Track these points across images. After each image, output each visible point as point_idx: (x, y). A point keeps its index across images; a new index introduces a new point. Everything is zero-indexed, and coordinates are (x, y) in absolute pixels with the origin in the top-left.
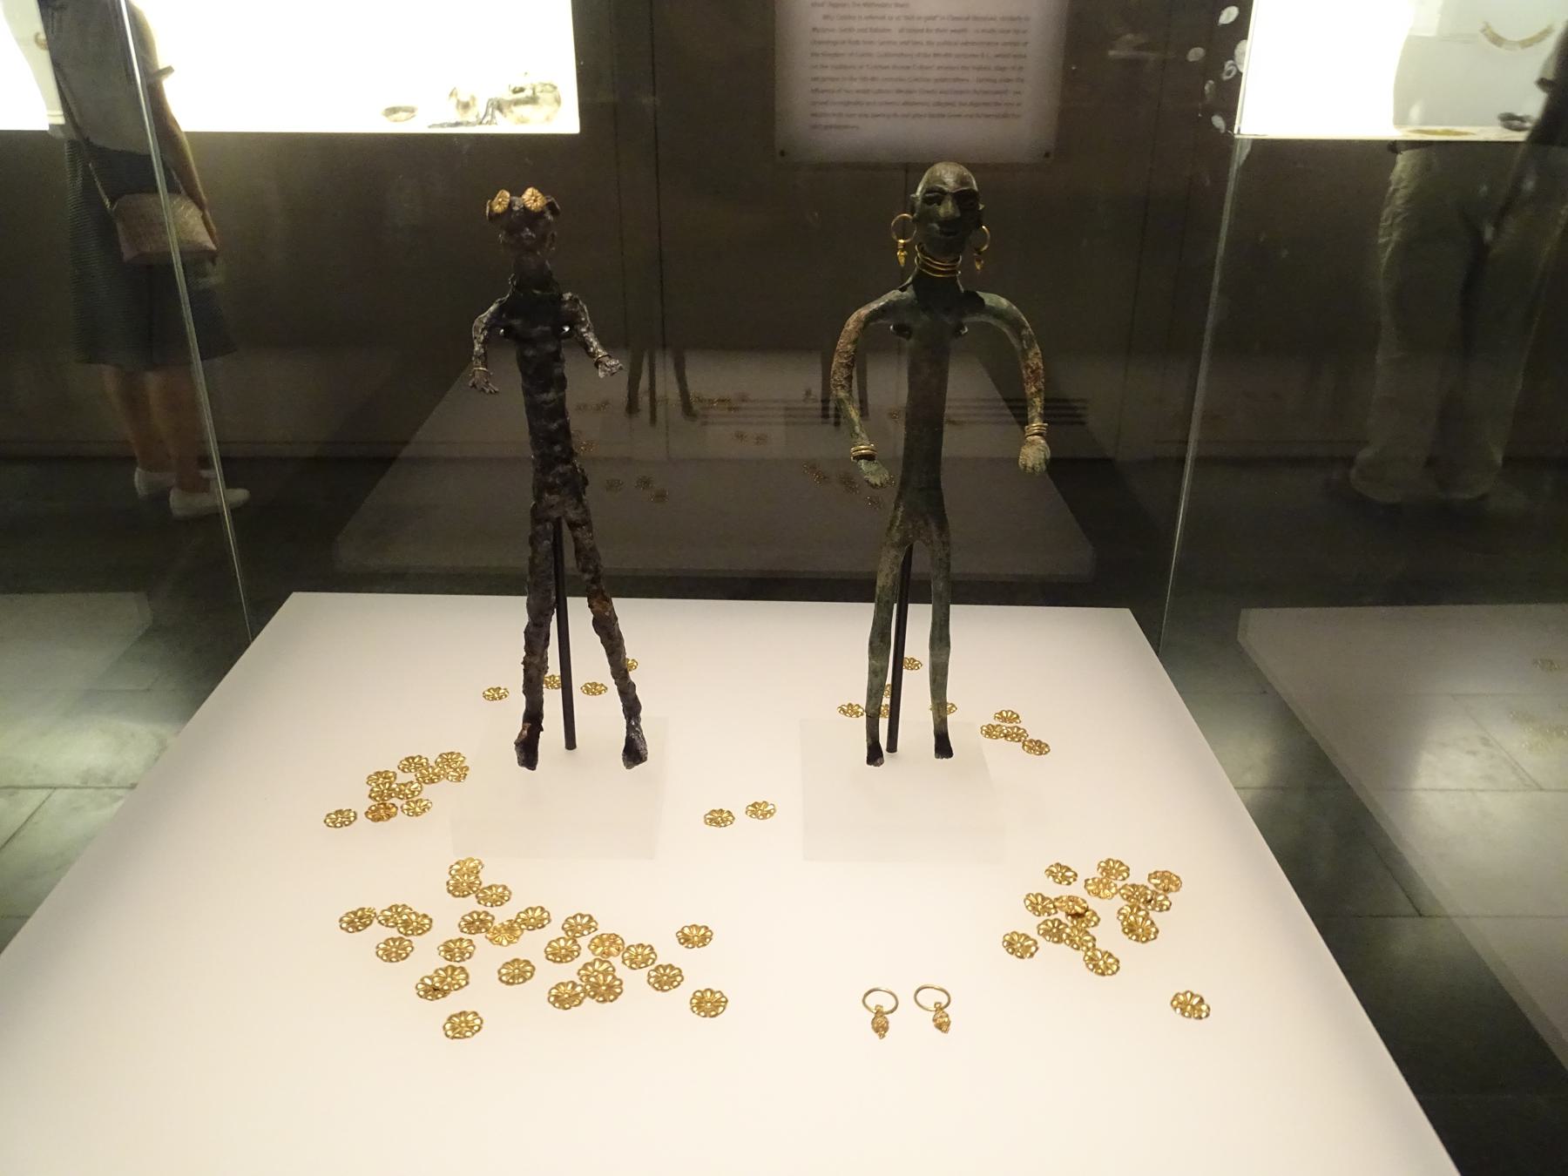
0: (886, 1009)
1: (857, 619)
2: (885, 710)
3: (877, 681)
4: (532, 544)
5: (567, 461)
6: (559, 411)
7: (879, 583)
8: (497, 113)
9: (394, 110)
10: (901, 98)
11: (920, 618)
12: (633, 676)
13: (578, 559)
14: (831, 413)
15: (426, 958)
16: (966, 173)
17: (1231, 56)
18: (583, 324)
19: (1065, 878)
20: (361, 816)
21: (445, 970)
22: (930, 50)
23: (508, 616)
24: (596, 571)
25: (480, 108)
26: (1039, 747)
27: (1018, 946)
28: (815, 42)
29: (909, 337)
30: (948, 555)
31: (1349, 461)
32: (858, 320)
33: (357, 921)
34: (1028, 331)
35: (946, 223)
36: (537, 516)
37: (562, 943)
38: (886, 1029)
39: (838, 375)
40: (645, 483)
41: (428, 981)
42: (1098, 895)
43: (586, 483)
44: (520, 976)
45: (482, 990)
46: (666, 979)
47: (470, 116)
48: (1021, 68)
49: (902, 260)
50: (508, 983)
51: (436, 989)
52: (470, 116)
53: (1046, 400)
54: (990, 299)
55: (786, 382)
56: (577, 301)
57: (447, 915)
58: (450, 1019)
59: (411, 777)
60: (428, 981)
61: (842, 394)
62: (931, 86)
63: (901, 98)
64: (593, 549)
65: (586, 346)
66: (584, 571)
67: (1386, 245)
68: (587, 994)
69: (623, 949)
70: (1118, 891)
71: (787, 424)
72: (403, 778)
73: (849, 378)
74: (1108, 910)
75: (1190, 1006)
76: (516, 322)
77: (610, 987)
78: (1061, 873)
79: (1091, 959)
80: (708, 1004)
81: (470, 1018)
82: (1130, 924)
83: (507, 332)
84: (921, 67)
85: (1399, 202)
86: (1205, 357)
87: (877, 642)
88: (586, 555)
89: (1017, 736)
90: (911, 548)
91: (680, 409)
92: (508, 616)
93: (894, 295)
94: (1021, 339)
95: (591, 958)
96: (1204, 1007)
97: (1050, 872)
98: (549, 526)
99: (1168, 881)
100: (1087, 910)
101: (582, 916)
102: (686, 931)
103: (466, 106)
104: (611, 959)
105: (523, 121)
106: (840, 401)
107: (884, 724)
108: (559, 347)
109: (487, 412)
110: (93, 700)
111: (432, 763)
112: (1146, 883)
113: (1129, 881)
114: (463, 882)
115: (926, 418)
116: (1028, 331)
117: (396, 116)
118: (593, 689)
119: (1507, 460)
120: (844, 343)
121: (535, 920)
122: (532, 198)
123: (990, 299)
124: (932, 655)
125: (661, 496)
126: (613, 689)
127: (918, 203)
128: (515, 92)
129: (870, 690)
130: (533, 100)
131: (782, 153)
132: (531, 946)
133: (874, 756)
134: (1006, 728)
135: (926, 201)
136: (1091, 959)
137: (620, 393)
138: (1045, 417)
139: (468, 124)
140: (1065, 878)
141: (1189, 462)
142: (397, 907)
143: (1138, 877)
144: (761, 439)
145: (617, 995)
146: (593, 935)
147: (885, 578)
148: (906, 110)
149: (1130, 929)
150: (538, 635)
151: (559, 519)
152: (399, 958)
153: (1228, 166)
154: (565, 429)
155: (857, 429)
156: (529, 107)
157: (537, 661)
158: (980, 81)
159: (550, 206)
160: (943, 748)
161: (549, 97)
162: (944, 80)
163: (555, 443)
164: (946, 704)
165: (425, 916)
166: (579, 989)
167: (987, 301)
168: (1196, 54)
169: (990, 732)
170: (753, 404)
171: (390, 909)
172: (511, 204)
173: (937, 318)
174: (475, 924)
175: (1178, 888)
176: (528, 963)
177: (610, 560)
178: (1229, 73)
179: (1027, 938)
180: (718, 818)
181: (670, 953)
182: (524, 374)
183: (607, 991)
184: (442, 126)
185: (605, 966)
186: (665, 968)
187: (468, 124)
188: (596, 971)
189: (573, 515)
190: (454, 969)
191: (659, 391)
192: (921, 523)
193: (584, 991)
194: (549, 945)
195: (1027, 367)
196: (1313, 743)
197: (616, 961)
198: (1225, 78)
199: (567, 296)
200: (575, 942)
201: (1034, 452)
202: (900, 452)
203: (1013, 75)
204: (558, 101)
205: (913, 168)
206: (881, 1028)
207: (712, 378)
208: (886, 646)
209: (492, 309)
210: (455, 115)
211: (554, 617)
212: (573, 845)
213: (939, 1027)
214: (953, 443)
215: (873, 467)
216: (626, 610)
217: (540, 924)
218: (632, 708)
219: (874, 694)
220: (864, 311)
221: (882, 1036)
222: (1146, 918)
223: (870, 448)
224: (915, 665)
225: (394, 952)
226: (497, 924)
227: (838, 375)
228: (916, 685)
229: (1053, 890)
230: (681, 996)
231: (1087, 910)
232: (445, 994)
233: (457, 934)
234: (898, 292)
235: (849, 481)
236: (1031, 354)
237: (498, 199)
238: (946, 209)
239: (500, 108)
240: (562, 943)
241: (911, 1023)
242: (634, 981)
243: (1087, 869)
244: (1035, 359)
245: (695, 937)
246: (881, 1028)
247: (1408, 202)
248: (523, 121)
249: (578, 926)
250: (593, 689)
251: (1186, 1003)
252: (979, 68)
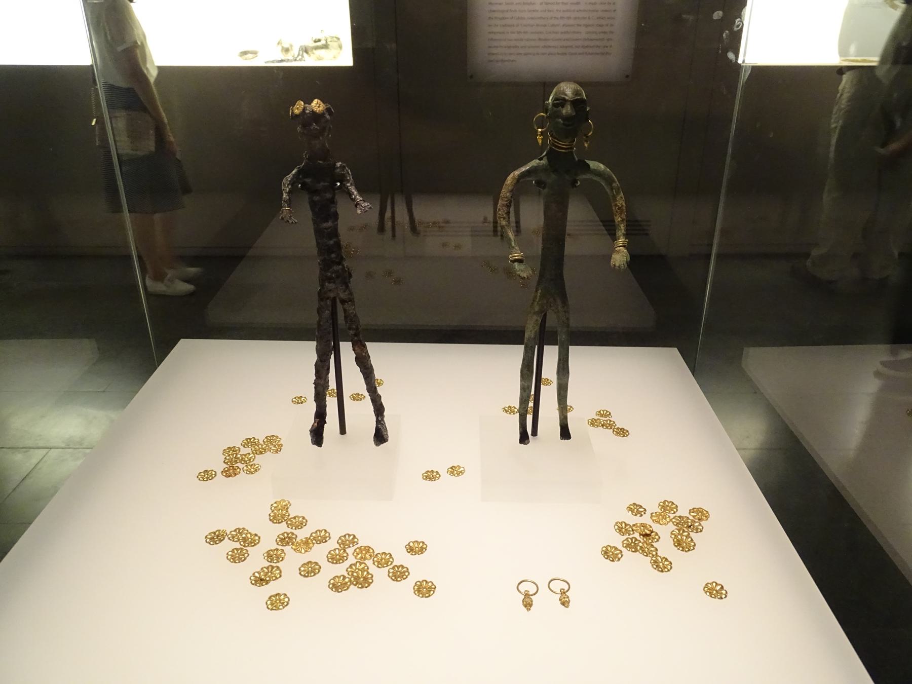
0: (531, 593)
1: (514, 355)
2: (530, 410)
3: (525, 394)
4: (318, 312)
5: (339, 263)
6: (334, 233)
7: (526, 336)
8: (305, 54)
9: (245, 53)
10: (542, 44)
11: (551, 354)
12: (380, 390)
13: (346, 322)
14: (497, 231)
15: (256, 560)
16: (579, 88)
17: (740, 16)
18: (348, 181)
19: (638, 512)
20: (219, 474)
21: (267, 568)
22: (559, 15)
23: (304, 354)
24: (357, 328)
25: (295, 51)
26: (623, 432)
27: (610, 554)
28: (491, 11)
29: (544, 188)
30: (568, 319)
31: (807, 255)
32: (514, 178)
33: (216, 538)
34: (616, 184)
35: (567, 119)
36: (322, 296)
37: (337, 551)
38: (531, 605)
39: (501, 212)
40: (390, 273)
41: (257, 575)
42: (658, 522)
43: (350, 276)
44: (312, 572)
45: (289, 581)
46: (399, 574)
47: (289, 56)
48: (612, 25)
49: (540, 142)
50: (305, 576)
51: (262, 580)
52: (289, 56)
53: (627, 226)
54: (593, 164)
55: (471, 213)
56: (344, 167)
57: (269, 534)
58: (270, 598)
59: (248, 450)
60: (257, 575)
61: (504, 223)
62: (559, 36)
63: (542, 44)
64: (355, 315)
65: (350, 194)
66: (350, 329)
67: (836, 127)
68: (351, 583)
69: (373, 555)
70: (671, 520)
71: (472, 236)
72: (244, 451)
73: (508, 213)
74: (665, 532)
75: (715, 591)
76: (308, 180)
77: (366, 579)
78: (636, 509)
79: (655, 562)
80: (424, 589)
81: (282, 597)
82: (678, 540)
83: (303, 185)
84: (553, 25)
85: (844, 102)
86: (722, 199)
87: (525, 371)
88: (351, 319)
89: (610, 425)
90: (545, 315)
91: (409, 229)
92: (304, 354)
93: (535, 163)
94: (612, 189)
95: (354, 561)
96: (724, 592)
97: (630, 509)
98: (329, 302)
99: (701, 514)
100: (652, 532)
101: (349, 535)
102: (411, 544)
103: (287, 50)
104: (366, 562)
105: (320, 59)
106: (502, 227)
107: (529, 418)
108: (334, 195)
109: (293, 229)
110: (69, 397)
111: (261, 442)
112: (688, 515)
113: (678, 514)
114: (279, 514)
115: (555, 236)
116: (616, 184)
117: (246, 56)
118: (357, 397)
119: (901, 254)
120: (505, 192)
121: (321, 537)
122: (317, 105)
123: (593, 164)
124: (558, 379)
125: (398, 281)
126: (368, 398)
127: (550, 107)
128: (315, 42)
129: (521, 399)
130: (326, 47)
131: (471, 77)
132: (319, 553)
133: (524, 439)
134: (603, 421)
135: (554, 105)
136: (655, 562)
137: (374, 219)
138: (627, 235)
139: (288, 60)
140: (638, 512)
141: (713, 258)
142: (239, 529)
143: (683, 511)
144: (457, 247)
145: (369, 584)
146: (356, 547)
147: (531, 331)
148: (544, 51)
149: (679, 544)
150: (323, 367)
151: (334, 298)
152: (241, 560)
153: (737, 82)
154: (338, 245)
155: (513, 244)
156: (323, 50)
157: (322, 382)
158: (588, 33)
159: (328, 110)
160: (565, 433)
161: (335, 44)
162: (567, 32)
163: (333, 252)
164: (567, 406)
165: (256, 535)
166: (347, 580)
168: (718, 15)
169: (593, 423)
170: (454, 226)
171: (235, 531)
172: (304, 109)
173: (563, 175)
174: (285, 540)
175: (707, 518)
176: (316, 564)
177: (365, 320)
178: (738, 26)
179: (616, 549)
180: (431, 476)
181: (401, 558)
182: (313, 210)
183: (364, 581)
184: (273, 62)
185: (363, 565)
186: (398, 567)
187: (288, 60)
188: (357, 568)
189: (343, 295)
190: (273, 567)
191: (397, 219)
192: (551, 300)
193: (350, 581)
194: (330, 553)
195: (616, 205)
196: (783, 422)
197: (369, 563)
198: (736, 29)
199: (338, 164)
200: (345, 551)
201: (620, 257)
202: (540, 252)
203: (607, 29)
204: (340, 47)
205: (547, 85)
206: (528, 605)
207: (427, 211)
208: (531, 373)
209: (294, 172)
210: (281, 56)
211: (333, 356)
212: (343, 492)
213: (563, 604)
214: (570, 248)
215: (522, 267)
216: (374, 349)
217: (324, 540)
218: (379, 410)
219: (524, 401)
220: (517, 173)
221: (529, 610)
222: (688, 536)
223: (520, 255)
224: (548, 382)
225: (237, 557)
226: (298, 539)
227: (501, 212)
228: (548, 395)
229: (632, 519)
230: (408, 584)
231: (652, 532)
232: (267, 582)
233: (275, 546)
234: (537, 161)
235: (510, 273)
236: (618, 198)
237: (297, 106)
238: (567, 110)
239: (306, 51)
240: (337, 551)
241: (546, 601)
242: (380, 575)
243: (652, 507)
244: (621, 201)
245: (417, 548)
246: (528, 605)
247: (849, 101)
248: (320, 59)
249: (348, 541)
250: (357, 397)
251: (713, 589)
252: (587, 26)
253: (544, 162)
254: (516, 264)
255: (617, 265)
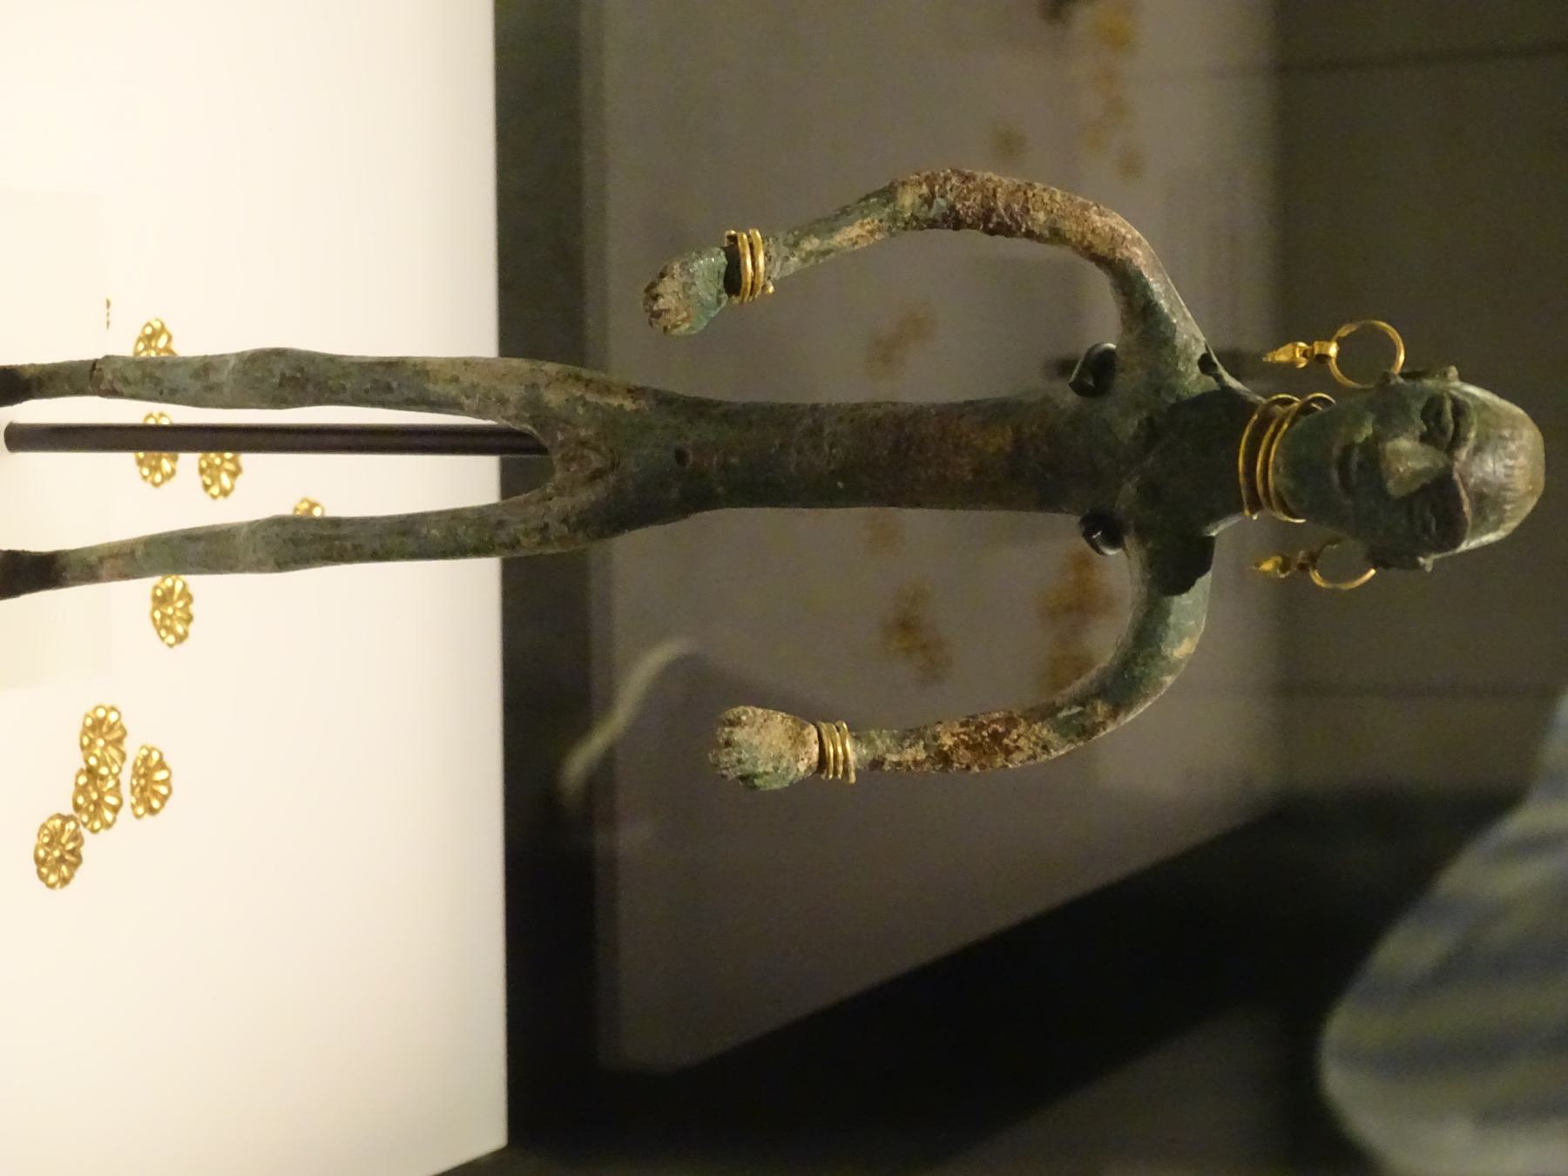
26: (58, 858)
29: (1079, 387)
32: (1115, 239)
35: (1373, 456)
49: (1282, 356)
87: (280, 367)
94: (1083, 700)
142: (74, 866)
167: (1183, 602)
169: (102, 730)
192: (596, 461)
228: (182, 497)
236: (1043, 731)
238: (1408, 454)
253: (1193, 381)
254: (720, 260)
255: (739, 735)
